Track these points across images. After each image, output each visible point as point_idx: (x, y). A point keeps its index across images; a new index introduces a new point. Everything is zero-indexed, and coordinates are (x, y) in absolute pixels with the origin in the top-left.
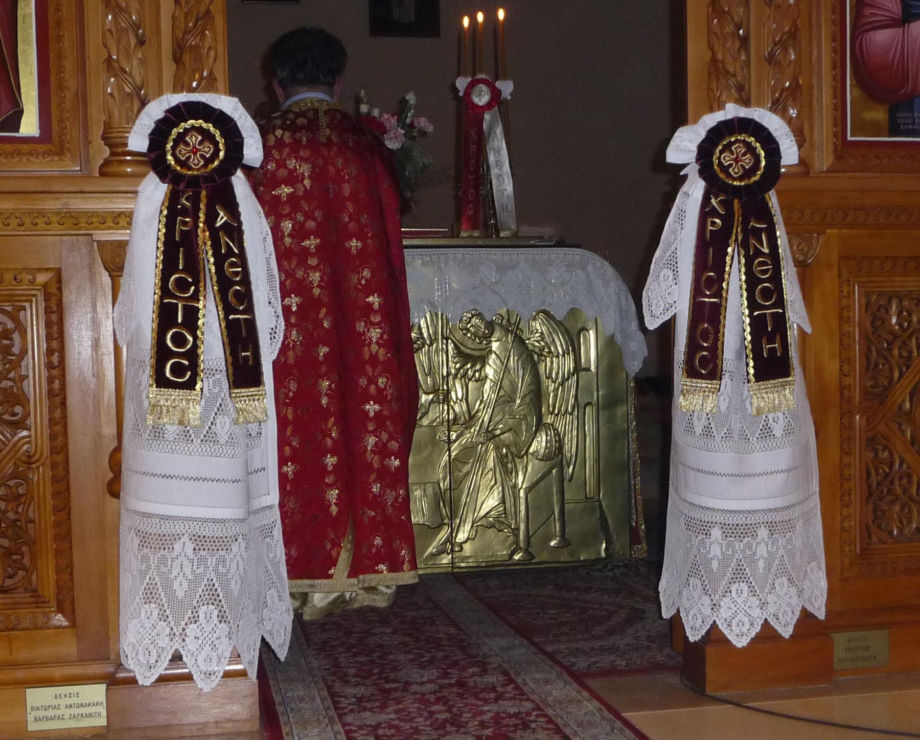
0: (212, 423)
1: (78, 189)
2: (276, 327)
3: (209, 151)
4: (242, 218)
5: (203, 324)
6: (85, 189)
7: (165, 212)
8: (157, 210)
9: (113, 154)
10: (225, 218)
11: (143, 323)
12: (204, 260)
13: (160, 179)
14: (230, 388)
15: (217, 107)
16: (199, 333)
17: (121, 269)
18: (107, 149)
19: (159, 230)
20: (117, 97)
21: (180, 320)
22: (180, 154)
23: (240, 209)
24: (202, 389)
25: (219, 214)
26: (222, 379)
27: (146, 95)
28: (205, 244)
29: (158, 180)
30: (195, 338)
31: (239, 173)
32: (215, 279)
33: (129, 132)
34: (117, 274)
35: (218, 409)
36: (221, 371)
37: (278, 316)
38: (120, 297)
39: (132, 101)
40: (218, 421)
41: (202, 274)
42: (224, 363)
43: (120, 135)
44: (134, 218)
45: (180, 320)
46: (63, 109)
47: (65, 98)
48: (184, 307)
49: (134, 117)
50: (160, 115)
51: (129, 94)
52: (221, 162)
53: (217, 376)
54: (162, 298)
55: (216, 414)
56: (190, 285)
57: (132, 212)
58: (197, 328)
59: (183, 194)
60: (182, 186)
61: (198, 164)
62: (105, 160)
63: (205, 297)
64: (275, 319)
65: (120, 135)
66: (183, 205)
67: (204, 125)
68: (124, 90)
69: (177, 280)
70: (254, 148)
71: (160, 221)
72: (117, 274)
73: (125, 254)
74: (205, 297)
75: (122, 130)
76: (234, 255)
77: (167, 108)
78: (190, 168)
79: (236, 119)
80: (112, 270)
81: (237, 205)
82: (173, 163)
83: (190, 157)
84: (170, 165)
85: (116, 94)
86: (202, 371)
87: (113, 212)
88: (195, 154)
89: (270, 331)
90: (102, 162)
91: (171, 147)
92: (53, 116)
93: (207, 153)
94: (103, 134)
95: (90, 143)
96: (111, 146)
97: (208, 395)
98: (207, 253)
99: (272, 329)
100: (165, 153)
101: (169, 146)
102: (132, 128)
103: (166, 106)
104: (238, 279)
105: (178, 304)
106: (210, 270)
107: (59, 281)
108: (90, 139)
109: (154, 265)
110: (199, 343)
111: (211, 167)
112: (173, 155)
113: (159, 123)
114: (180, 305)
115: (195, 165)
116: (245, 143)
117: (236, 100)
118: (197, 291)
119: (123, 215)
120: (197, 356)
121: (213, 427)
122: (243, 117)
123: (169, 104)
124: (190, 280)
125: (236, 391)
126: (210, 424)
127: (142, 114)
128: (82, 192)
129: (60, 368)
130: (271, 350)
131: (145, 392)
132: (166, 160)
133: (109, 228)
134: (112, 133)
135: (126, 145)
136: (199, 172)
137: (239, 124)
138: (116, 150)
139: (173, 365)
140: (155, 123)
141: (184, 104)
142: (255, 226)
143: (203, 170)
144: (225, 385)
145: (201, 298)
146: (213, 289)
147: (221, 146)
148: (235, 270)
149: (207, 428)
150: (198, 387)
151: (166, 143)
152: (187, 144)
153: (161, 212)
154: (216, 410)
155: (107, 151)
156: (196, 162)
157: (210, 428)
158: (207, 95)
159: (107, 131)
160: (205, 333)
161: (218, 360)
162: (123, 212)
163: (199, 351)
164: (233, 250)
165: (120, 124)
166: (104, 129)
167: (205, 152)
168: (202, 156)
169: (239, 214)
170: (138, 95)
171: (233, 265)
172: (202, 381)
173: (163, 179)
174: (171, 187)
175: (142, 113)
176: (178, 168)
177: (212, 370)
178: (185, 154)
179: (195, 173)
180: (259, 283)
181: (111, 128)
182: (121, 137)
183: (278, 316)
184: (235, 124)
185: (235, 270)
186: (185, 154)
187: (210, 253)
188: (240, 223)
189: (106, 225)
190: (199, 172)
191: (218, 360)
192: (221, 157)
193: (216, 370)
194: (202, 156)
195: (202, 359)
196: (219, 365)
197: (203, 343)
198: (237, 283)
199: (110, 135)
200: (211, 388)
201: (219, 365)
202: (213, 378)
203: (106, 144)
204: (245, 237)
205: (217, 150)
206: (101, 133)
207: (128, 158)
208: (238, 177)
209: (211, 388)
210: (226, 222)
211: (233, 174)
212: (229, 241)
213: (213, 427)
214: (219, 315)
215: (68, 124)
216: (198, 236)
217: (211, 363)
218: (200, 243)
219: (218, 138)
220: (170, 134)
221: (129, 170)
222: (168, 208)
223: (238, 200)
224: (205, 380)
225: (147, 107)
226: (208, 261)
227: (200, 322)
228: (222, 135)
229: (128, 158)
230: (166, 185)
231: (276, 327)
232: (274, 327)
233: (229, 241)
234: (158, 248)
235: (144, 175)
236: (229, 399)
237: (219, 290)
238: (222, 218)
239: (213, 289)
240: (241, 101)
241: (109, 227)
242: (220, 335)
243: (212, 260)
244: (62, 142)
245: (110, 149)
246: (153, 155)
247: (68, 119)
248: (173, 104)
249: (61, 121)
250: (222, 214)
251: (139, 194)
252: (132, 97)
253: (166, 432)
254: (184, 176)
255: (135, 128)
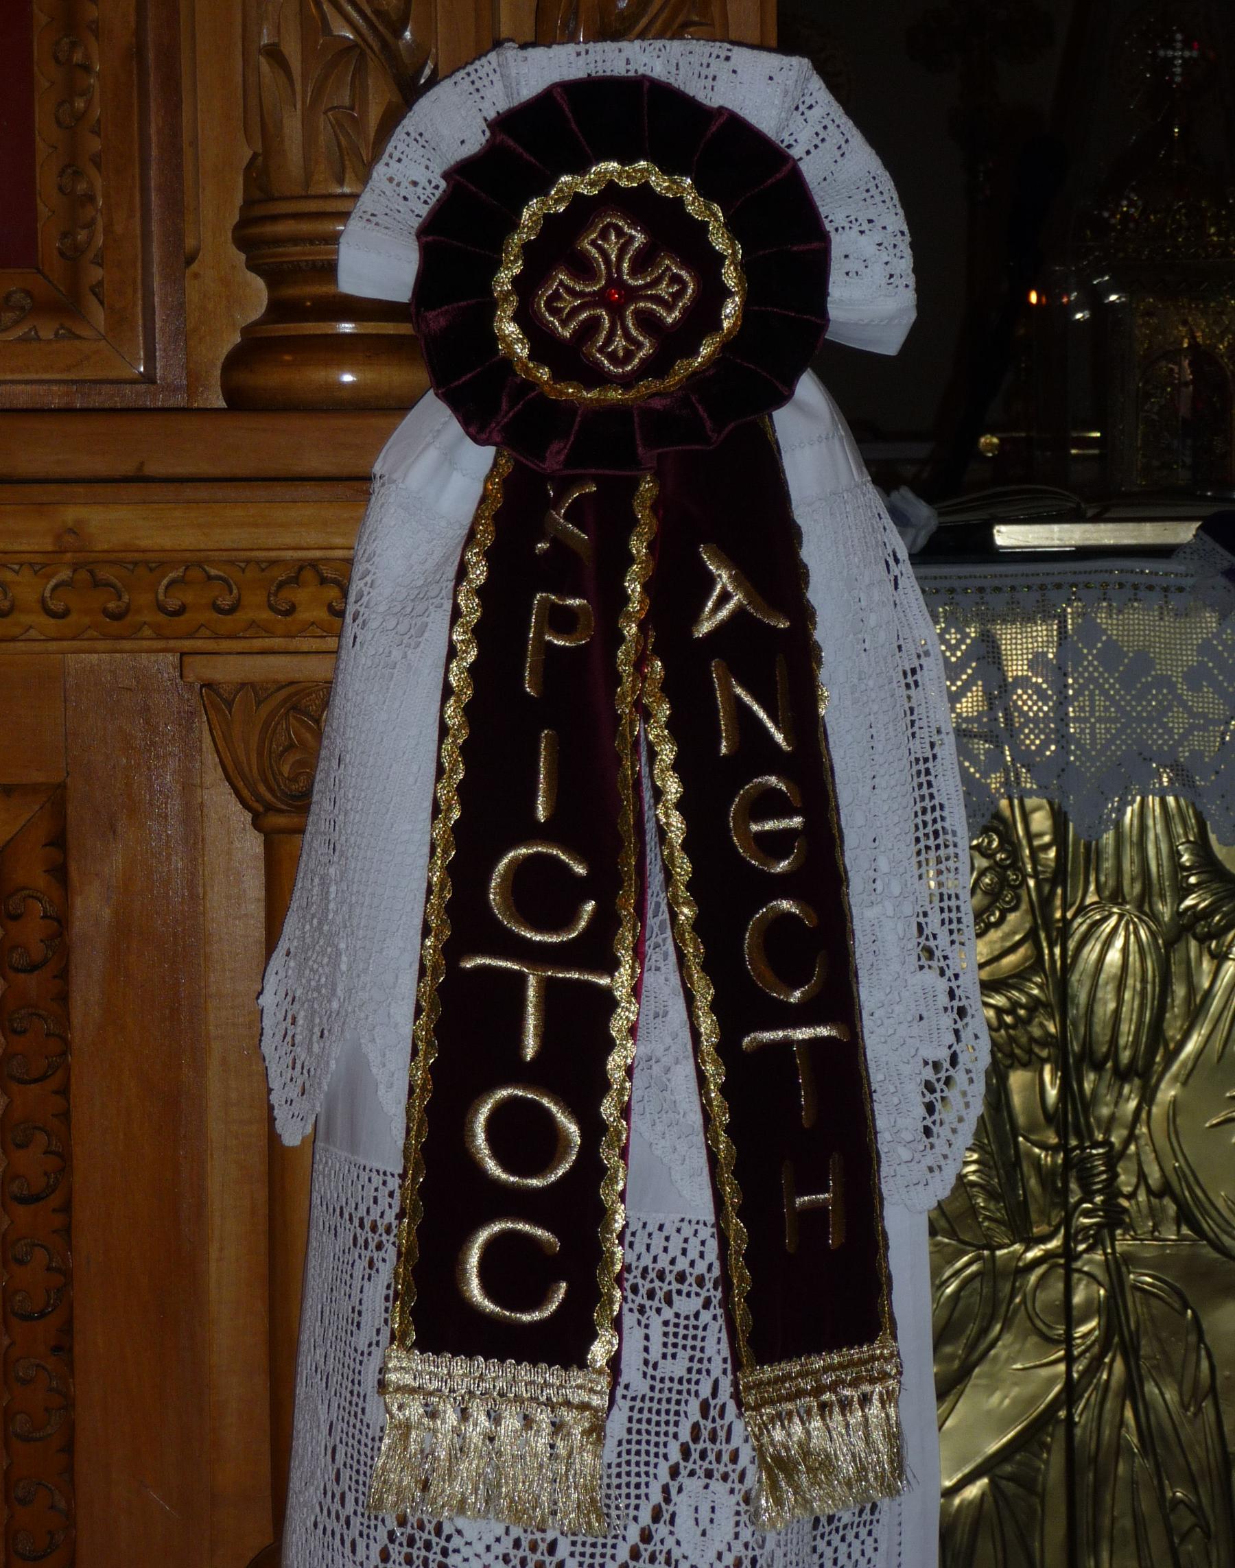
0: (657, 1516)
1: (126, 467)
2: (954, 1060)
3: (677, 296)
4: (816, 595)
5: (629, 1071)
6: (152, 469)
7: (479, 574)
8: (446, 558)
9: (279, 309)
10: (737, 598)
11: (373, 1056)
12: (637, 784)
13: (466, 423)
14: (737, 1365)
15: (713, 99)
16: (608, 1109)
17: (301, 802)
18: (259, 283)
19: (452, 653)
20: (296, 65)
21: (530, 1047)
22: (555, 312)
23: (808, 554)
24: (615, 1363)
25: (711, 580)
26: (706, 1316)
27: (421, 51)
28: (647, 715)
29: (456, 427)
30: (594, 1129)
31: (808, 388)
32: (684, 867)
33: (344, 216)
34: (281, 821)
35: (686, 1452)
36: (700, 1281)
37: (962, 1012)
38: (291, 926)
39: (360, 71)
40: (682, 1505)
41: (631, 844)
42: (713, 1246)
43: (306, 227)
44: (356, 587)
45: (530, 1047)
46: (80, 117)
47: (87, 68)
48: (549, 989)
49: (366, 154)
50: (474, 140)
51: (351, 47)
52: (730, 347)
53: (686, 1306)
54: (452, 951)
55: (674, 1472)
56: (581, 889)
57: (350, 562)
58: (604, 1086)
59: (561, 494)
60: (555, 458)
61: (629, 356)
62: (245, 331)
63: (639, 954)
64: (947, 1021)
65: (306, 227)
66: (559, 544)
67: (660, 183)
68: (326, 27)
69: (522, 868)
70: (878, 273)
71: (456, 613)
72: (281, 821)
73: (319, 735)
74: (639, 954)
75: (313, 206)
76: (770, 759)
77: (503, 106)
78: (598, 377)
79: (796, 152)
80: (269, 808)
81: (791, 535)
82: (522, 351)
83: (592, 325)
84: (507, 363)
85: (292, 50)
86: (619, 1280)
87: (273, 563)
88: (617, 313)
89: (929, 1074)
90: (237, 339)
91: (515, 280)
92: (40, 144)
93: (670, 308)
94: (238, 227)
95: (190, 260)
96: (273, 277)
97: (640, 1386)
98: (653, 755)
99: (937, 1066)
100: (489, 306)
101: (504, 278)
102: (355, 197)
103: (497, 101)
104: (783, 866)
105: (521, 979)
106: (662, 832)
107: (59, 841)
108: (190, 243)
109: (428, 805)
110: (609, 1157)
111: (683, 368)
112: (523, 317)
113: (462, 174)
114: (532, 980)
115: (612, 357)
116: (836, 252)
117: (797, 66)
118: (605, 923)
119: (308, 575)
120: (602, 1214)
121: (661, 1530)
122: (834, 137)
123: (508, 96)
124: (580, 870)
125: (768, 1372)
126: (645, 1517)
127: (398, 141)
128: (140, 479)
129: (55, 1200)
130: (929, 1160)
131: (373, 1365)
132: (493, 339)
133: (257, 628)
134: (275, 218)
135: (329, 270)
136: (631, 395)
137: (811, 171)
138: (290, 292)
139: (490, 1249)
140: (446, 176)
141: (570, 89)
142: (873, 620)
143: (648, 386)
144: (716, 1346)
145: (626, 957)
146: (674, 916)
147: (730, 276)
148: (770, 825)
149: (633, 1534)
150: (599, 1352)
151: (496, 265)
152: (584, 268)
153: (462, 573)
154: (675, 1455)
155: (257, 293)
156: (619, 343)
157: (646, 1536)
158: (676, 47)
159: (259, 211)
160: (636, 1108)
161: (687, 1231)
162: (313, 564)
163: (607, 1195)
164: (770, 738)
165: (307, 184)
166: (248, 203)
167: (658, 300)
168: (648, 322)
169: (798, 575)
170: (389, 51)
171: (770, 804)
172: (617, 1324)
173: (477, 428)
174: (506, 468)
175: (400, 132)
176: (544, 374)
177: (661, 1276)
178: (575, 311)
179: (616, 395)
180: (883, 864)
181: (272, 199)
182: (311, 240)
183: (962, 1012)
184: (796, 177)
185: (770, 825)
186: (575, 311)
187: (667, 753)
188: (803, 615)
189: (242, 616)
190: (631, 395)
191: (687, 1231)
192: (726, 324)
193: (681, 1277)
194: (648, 322)
195: (618, 1226)
196: (693, 1254)
197: (624, 1154)
198: (782, 886)
199: (270, 229)
200: (655, 1355)
201: (693, 1254)
202: (668, 1313)
203: (252, 266)
204: (823, 675)
205: (713, 294)
206: (235, 218)
207: (347, 327)
208: (803, 409)
209: (655, 1355)
210: (739, 612)
211: (783, 396)
212: (747, 699)
213: (661, 1530)
214: (696, 1035)
215: (99, 184)
216: (617, 680)
217: (658, 1242)
218: (624, 709)
219: (720, 242)
220: (514, 225)
221: (348, 378)
222: (489, 555)
223: (802, 513)
224: (629, 1320)
225: (424, 105)
226: (658, 794)
227: (615, 1062)
228: (734, 228)
229: (347, 327)
230: (490, 451)
231: (954, 1060)
232: (943, 1055)
233: (747, 699)
234: (444, 731)
235: (401, 406)
236: (731, 1408)
237: (698, 925)
238: (725, 597)
239: (674, 916)
240: (821, 68)
241: (253, 624)
242: (697, 1118)
243: (673, 788)
244: (73, 256)
245: (271, 285)
246: (437, 320)
247: (96, 161)
248: (529, 89)
249: (72, 168)
250: (723, 578)
251: (376, 485)
252: (362, 55)
253: (457, 1542)
254: (569, 409)
255: (368, 201)
